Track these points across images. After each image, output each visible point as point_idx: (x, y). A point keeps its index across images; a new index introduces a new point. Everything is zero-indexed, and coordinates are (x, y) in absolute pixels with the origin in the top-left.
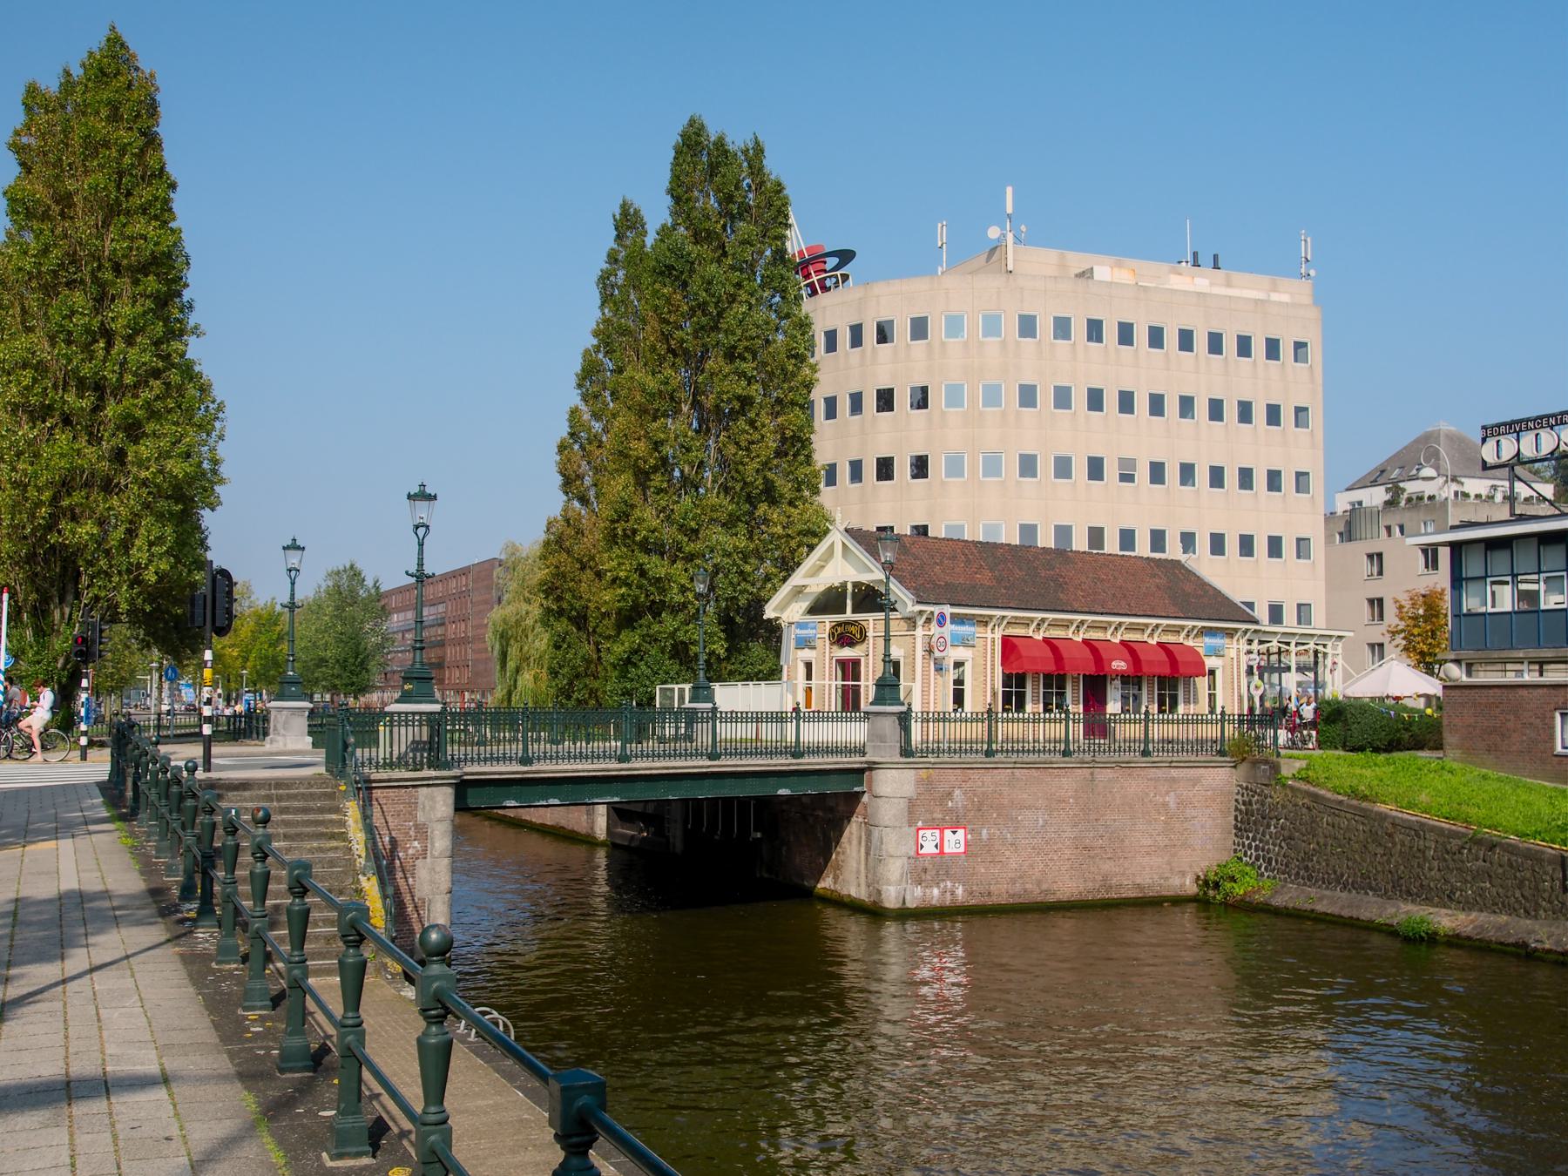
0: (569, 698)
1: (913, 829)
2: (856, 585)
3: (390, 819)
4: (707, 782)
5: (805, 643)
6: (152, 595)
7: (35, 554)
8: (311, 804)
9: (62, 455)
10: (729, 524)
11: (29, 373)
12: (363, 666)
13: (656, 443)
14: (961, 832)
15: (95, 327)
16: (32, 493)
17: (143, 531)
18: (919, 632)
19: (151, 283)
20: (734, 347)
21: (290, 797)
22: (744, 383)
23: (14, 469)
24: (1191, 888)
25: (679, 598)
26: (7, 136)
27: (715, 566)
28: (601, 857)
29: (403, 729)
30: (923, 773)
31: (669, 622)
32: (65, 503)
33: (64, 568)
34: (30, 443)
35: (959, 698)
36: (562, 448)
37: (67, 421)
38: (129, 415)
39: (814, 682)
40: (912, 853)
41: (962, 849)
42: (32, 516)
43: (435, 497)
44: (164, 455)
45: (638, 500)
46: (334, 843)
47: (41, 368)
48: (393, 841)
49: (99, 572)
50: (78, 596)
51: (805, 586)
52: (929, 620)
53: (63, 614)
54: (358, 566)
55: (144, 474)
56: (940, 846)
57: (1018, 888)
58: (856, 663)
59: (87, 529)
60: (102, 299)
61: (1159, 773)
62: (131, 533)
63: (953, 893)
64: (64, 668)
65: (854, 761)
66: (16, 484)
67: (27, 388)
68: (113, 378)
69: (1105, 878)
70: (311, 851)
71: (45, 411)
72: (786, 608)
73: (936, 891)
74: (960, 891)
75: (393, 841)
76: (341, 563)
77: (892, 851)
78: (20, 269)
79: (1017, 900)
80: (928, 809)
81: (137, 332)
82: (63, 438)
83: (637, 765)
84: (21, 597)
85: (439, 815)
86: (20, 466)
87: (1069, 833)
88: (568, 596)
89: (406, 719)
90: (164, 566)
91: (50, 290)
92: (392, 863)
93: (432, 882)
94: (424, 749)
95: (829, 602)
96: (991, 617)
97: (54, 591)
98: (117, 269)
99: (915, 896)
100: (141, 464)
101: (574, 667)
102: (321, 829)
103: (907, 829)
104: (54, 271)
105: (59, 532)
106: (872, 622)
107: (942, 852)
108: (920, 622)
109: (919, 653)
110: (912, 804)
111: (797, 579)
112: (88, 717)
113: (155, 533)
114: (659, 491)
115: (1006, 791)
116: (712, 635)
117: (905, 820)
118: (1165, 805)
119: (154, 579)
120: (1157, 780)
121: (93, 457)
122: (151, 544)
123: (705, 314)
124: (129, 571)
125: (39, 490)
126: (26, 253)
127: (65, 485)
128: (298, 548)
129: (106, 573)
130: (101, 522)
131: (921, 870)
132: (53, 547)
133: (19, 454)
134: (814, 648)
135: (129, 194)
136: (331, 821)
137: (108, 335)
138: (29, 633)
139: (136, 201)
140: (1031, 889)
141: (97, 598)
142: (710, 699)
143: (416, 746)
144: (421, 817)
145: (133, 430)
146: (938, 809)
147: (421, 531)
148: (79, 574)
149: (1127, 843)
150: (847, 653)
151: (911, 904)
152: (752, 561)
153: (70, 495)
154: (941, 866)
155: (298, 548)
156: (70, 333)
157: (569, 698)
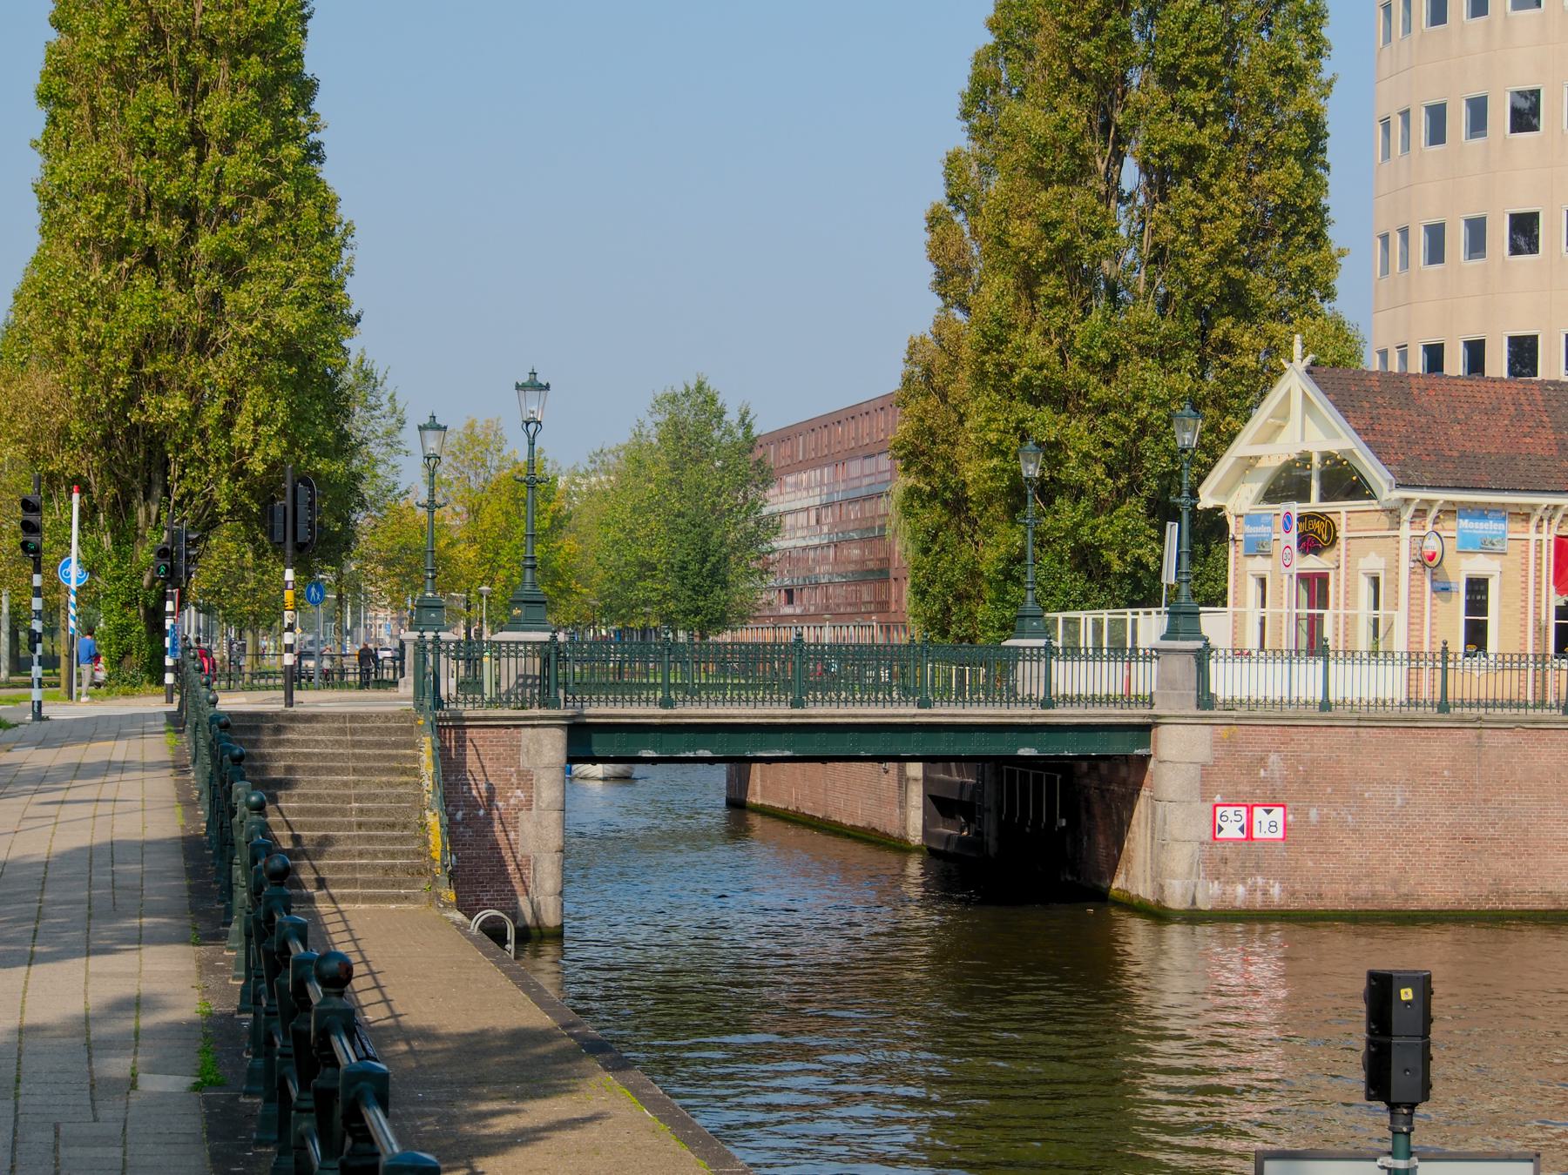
0: (944, 633)
1: (1208, 806)
2: (1326, 456)
3: (487, 763)
4: (915, 736)
5: (1257, 549)
6: (265, 491)
7: (112, 436)
8: (386, 738)
9: (142, 308)
10: (1165, 354)
11: (101, 198)
12: (717, 577)
13: (1046, 225)
14: (1278, 813)
16: (107, 357)
17: (247, 406)
18: (1405, 531)
19: (255, 67)
20: (1175, 66)
21: (364, 731)
22: (1190, 125)
23: (84, 327)
27: (1142, 422)
28: (914, 868)
29: (512, 660)
31: (1067, 512)
32: (148, 370)
33: (149, 453)
34: (103, 291)
35: (1476, 635)
36: (934, 220)
37: (150, 259)
38: (226, 250)
39: (1381, 612)
40: (1207, 836)
41: (1280, 834)
42: (108, 384)
43: (547, 387)
44: (272, 302)
45: (1023, 316)
46: (405, 779)
47: (118, 188)
48: (491, 789)
49: (192, 460)
50: (167, 491)
51: (1258, 458)
52: (1421, 513)
53: (148, 515)
54: (712, 385)
55: (246, 330)
56: (1248, 828)
57: (1364, 888)
58: (1323, 579)
59: (176, 403)
60: (194, 91)
62: (232, 407)
63: (1265, 893)
64: (151, 587)
65: (1136, 715)
66: (87, 347)
67: (99, 218)
68: (206, 199)
69: (1497, 881)
70: (380, 785)
71: (121, 249)
72: (1230, 490)
73: (1240, 890)
74: (1276, 890)
75: (491, 789)
76: (680, 380)
78: (88, 56)
79: (1361, 906)
80: (1234, 779)
82: (144, 283)
83: (813, 712)
84: (96, 491)
85: (546, 761)
86: (91, 323)
88: (939, 467)
89: (513, 648)
90: (274, 452)
91: (124, 82)
92: (489, 813)
94: (533, 686)
95: (1287, 484)
96: (1534, 507)
97: (136, 484)
98: (211, 47)
99: (1209, 895)
100: (245, 317)
101: (949, 585)
102: (395, 764)
103: (1198, 805)
104: (131, 57)
105: (142, 407)
106: (1342, 511)
107: (1250, 837)
108: (1407, 515)
109: (1405, 564)
110: (1207, 774)
111: (1241, 447)
112: (173, 649)
113: (264, 406)
114: (1053, 302)
116: (1136, 532)
119: (260, 468)
121: (179, 306)
122: (258, 423)
124: (230, 459)
125: (118, 354)
126: (95, 32)
127: (150, 343)
128: (439, 428)
129: (201, 461)
130: (192, 392)
131: (1218, 858)
132: (135, 427)
133: (90, 304)
134: (1268, 555)
136: (404, 756)
137: (198, 139)
138: (107, 540)
140: (1384, 892)
141: (190, 494)
142: (1196, 634)
144: (525, 763)
145: (231, 268)
147: (532, 427)
148: (168, 463)
150: (1312, 563)
151: (1204, 904)
152: (1209, 411)
153: (154, 359)
155: (439, 428)
156: (152, 142)
157: (944, 633)
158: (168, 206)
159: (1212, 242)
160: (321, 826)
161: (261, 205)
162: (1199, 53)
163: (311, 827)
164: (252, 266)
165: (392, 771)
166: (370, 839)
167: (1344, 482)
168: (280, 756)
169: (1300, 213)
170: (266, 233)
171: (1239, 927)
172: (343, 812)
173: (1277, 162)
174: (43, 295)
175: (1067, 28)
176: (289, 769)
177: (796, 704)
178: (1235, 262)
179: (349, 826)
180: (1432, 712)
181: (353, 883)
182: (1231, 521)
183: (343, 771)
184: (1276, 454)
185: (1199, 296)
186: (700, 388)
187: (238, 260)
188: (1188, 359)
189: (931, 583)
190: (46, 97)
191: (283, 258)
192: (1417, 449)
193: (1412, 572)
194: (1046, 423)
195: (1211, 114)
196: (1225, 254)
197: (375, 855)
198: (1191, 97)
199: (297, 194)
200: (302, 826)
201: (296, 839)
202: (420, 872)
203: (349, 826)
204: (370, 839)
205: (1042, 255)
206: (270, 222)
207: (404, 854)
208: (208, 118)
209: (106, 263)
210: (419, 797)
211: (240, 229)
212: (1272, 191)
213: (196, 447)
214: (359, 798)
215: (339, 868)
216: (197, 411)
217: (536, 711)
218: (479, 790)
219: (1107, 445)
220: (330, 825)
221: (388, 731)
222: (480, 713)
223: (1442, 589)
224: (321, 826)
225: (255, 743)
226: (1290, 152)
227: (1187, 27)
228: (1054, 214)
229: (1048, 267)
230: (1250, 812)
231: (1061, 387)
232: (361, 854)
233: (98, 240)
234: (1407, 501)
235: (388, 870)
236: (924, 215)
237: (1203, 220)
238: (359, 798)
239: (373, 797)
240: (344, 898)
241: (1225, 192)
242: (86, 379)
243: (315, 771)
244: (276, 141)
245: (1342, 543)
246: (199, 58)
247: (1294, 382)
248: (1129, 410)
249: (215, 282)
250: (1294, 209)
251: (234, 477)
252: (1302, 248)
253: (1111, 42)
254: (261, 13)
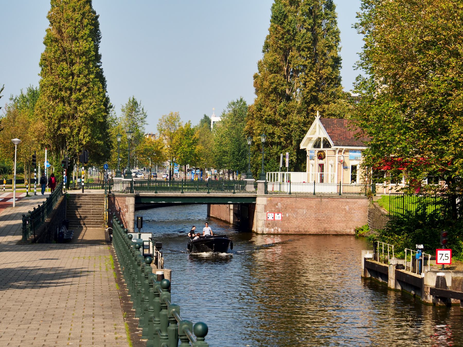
1: (266, 213)
5: (312, 158)
11: (52, 87)
14: (280, 214)
15: (69, 72)
16: (53, 120)
17: (82, 130)
18: (337, 155)
19: (84, 59)
23: (49, 114)
24: (353, 232)
25: (277, 140)
26: (46, 14)
30: (269, 198)
34: (53, 106)
40: (266, 219)
44: (87, 108)
47: (56, 85)
48: (120, 208)
50: (66, 148)
55: (81, 115)
56: (274, 217)
57: (297, 230)
58: (323, 165)
59: (68, 130)
61: (343, 200)
62: (79, 130)
63: (277, 230)
66: (49, 118)
67: (52, 91)
68: (74, 87)
69: (325, 228)
71: (56, 98)
72: (306, 145)
75: (120, 208)
77: (260, 219)
81: (80, 73)
82: (61, 105)
86: (50, 113)
87: (314, 216)
90: (88, 140)
91: (58, 62)
93: (129, 218)
99: (266, 230)
103: (264, 213)
106: (326, 150)
107: (274, 219)
108: (337, 151)
109: (337, 162)
110: (266, 207)
111: (308, 135)
113: (85, 130)
114: (273, 100)
115: (294, 204)
117: (263, 211)
118: (345, 209)
120: (343, 202)
122: (84, 133)
123: (289, 34)
124: (78, 141)
125: (55, 120)
130: (71, 128)
135: (78, 33)
137: (72, 74)
139: (80, 35)
143: (127, 188)
144: (127, 204)
145: (79, 102)
146: (273, 208)
149: (332, 219)
154: (274, 223)
156: (63, 75)
158: (66, 89)
159: (308, 87)
160: (85, 214)
161: (85, 88)
162: (306, 43)
163: (84, 214)
164: (83, 101)
165: (99, 205)
166: (94, 217)
167: (327, 145)
168: (78, 202)
169: (332, 79)
170: (86, 94)
171: (272, 236)
172: (90, 212)
173: (326, 67)
174: (40, 107)
175: (276, 37)
176: (81, 204)
177: (208, 193)
178: (314, 91)
179: (90, 214)
180: (313, 195)
181: (90, 224)
182: (307, 152)
183: (90, 205)
184: (315, 138)
185: (306, 99)
186: (241, 100)
187: (80, 100)
188: (304, 114)
189: (253, 164)
190: (41, 65)
191: (90, 99)
192: (341, 137)
193: (338, 164)
194: (270, 128)
195: (308, 57)
196: (311, 90)
197: (94, 219)
198: (303, 53)
199: (93, 85)
200: (82, 214)
201: (80, 217)
202: (102, 222)
203: (90, 214)
204: (94, 217)
205: (270, 90)
206: (87, 91)
207: (100, 219)
208: (74, 70)
209: (53, 101)
210: (103, 209)
211: (81, 93)
212: (324, 74)
213: (72, 139)
214: (93, 209)
215: (88, 222)
216: (72, 132)
217: (129, 194)
218: (118, 209)
219: (285, 133)
220: (87, 214)
221: (99, 197)
222: (118, 194)
223: (345, 168)
224: (85, 214)
225: (74, 200)
226: (329, 65)
227: (303, 37)
228: (272, 81)
229: (272, 92)
230: (274, 214)
231: (274, 120)
232: (92, 219)
233: (52, 96)
234: (337, 149)
235: (97, 222)
236: (253, 76)
237: (307, 82)
238: (93, 209)
239: (95, 209)
240: (88, 227)
241: (312, 75)
242: (49, 124)
243: (85, 205)
244: (89, 74)
245: (326, 157)
246: (72, 57)
247: (317, 122)
248: (290, 125)
249: (75, 104)
250: (330, 78)
251: (79, 145)
252: (333, 87)
253: (286, 41)
254: (85, 48)
